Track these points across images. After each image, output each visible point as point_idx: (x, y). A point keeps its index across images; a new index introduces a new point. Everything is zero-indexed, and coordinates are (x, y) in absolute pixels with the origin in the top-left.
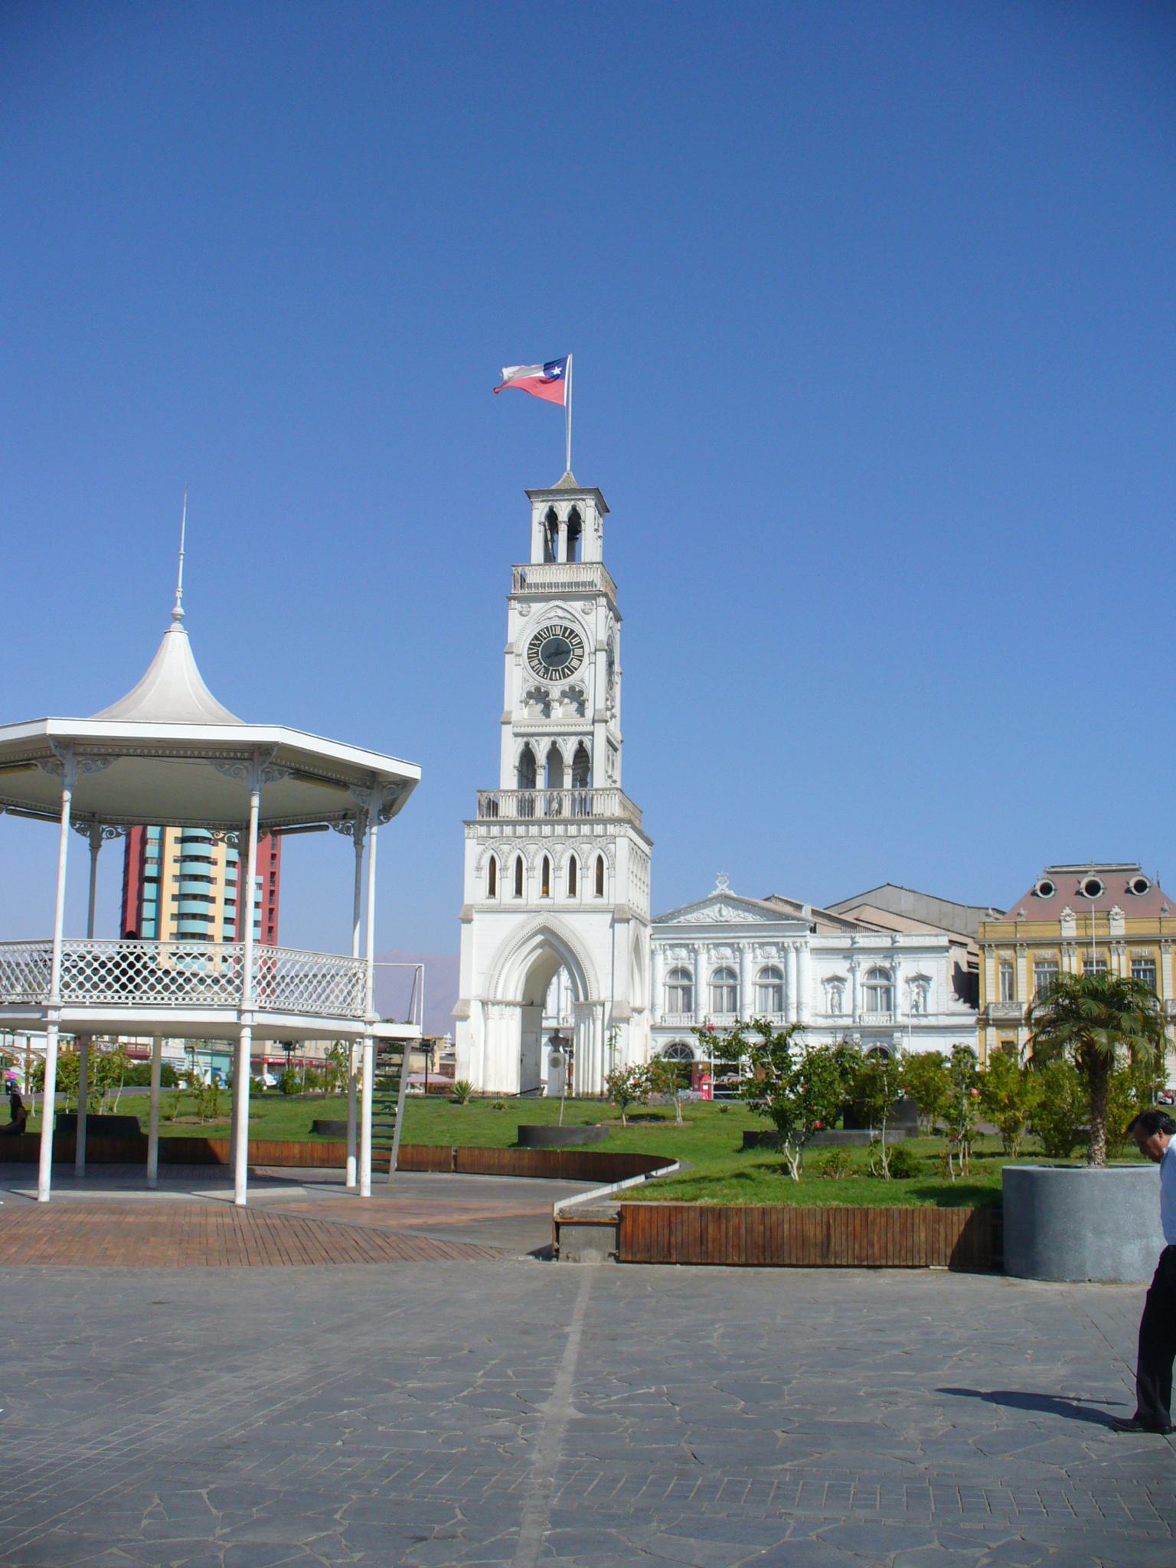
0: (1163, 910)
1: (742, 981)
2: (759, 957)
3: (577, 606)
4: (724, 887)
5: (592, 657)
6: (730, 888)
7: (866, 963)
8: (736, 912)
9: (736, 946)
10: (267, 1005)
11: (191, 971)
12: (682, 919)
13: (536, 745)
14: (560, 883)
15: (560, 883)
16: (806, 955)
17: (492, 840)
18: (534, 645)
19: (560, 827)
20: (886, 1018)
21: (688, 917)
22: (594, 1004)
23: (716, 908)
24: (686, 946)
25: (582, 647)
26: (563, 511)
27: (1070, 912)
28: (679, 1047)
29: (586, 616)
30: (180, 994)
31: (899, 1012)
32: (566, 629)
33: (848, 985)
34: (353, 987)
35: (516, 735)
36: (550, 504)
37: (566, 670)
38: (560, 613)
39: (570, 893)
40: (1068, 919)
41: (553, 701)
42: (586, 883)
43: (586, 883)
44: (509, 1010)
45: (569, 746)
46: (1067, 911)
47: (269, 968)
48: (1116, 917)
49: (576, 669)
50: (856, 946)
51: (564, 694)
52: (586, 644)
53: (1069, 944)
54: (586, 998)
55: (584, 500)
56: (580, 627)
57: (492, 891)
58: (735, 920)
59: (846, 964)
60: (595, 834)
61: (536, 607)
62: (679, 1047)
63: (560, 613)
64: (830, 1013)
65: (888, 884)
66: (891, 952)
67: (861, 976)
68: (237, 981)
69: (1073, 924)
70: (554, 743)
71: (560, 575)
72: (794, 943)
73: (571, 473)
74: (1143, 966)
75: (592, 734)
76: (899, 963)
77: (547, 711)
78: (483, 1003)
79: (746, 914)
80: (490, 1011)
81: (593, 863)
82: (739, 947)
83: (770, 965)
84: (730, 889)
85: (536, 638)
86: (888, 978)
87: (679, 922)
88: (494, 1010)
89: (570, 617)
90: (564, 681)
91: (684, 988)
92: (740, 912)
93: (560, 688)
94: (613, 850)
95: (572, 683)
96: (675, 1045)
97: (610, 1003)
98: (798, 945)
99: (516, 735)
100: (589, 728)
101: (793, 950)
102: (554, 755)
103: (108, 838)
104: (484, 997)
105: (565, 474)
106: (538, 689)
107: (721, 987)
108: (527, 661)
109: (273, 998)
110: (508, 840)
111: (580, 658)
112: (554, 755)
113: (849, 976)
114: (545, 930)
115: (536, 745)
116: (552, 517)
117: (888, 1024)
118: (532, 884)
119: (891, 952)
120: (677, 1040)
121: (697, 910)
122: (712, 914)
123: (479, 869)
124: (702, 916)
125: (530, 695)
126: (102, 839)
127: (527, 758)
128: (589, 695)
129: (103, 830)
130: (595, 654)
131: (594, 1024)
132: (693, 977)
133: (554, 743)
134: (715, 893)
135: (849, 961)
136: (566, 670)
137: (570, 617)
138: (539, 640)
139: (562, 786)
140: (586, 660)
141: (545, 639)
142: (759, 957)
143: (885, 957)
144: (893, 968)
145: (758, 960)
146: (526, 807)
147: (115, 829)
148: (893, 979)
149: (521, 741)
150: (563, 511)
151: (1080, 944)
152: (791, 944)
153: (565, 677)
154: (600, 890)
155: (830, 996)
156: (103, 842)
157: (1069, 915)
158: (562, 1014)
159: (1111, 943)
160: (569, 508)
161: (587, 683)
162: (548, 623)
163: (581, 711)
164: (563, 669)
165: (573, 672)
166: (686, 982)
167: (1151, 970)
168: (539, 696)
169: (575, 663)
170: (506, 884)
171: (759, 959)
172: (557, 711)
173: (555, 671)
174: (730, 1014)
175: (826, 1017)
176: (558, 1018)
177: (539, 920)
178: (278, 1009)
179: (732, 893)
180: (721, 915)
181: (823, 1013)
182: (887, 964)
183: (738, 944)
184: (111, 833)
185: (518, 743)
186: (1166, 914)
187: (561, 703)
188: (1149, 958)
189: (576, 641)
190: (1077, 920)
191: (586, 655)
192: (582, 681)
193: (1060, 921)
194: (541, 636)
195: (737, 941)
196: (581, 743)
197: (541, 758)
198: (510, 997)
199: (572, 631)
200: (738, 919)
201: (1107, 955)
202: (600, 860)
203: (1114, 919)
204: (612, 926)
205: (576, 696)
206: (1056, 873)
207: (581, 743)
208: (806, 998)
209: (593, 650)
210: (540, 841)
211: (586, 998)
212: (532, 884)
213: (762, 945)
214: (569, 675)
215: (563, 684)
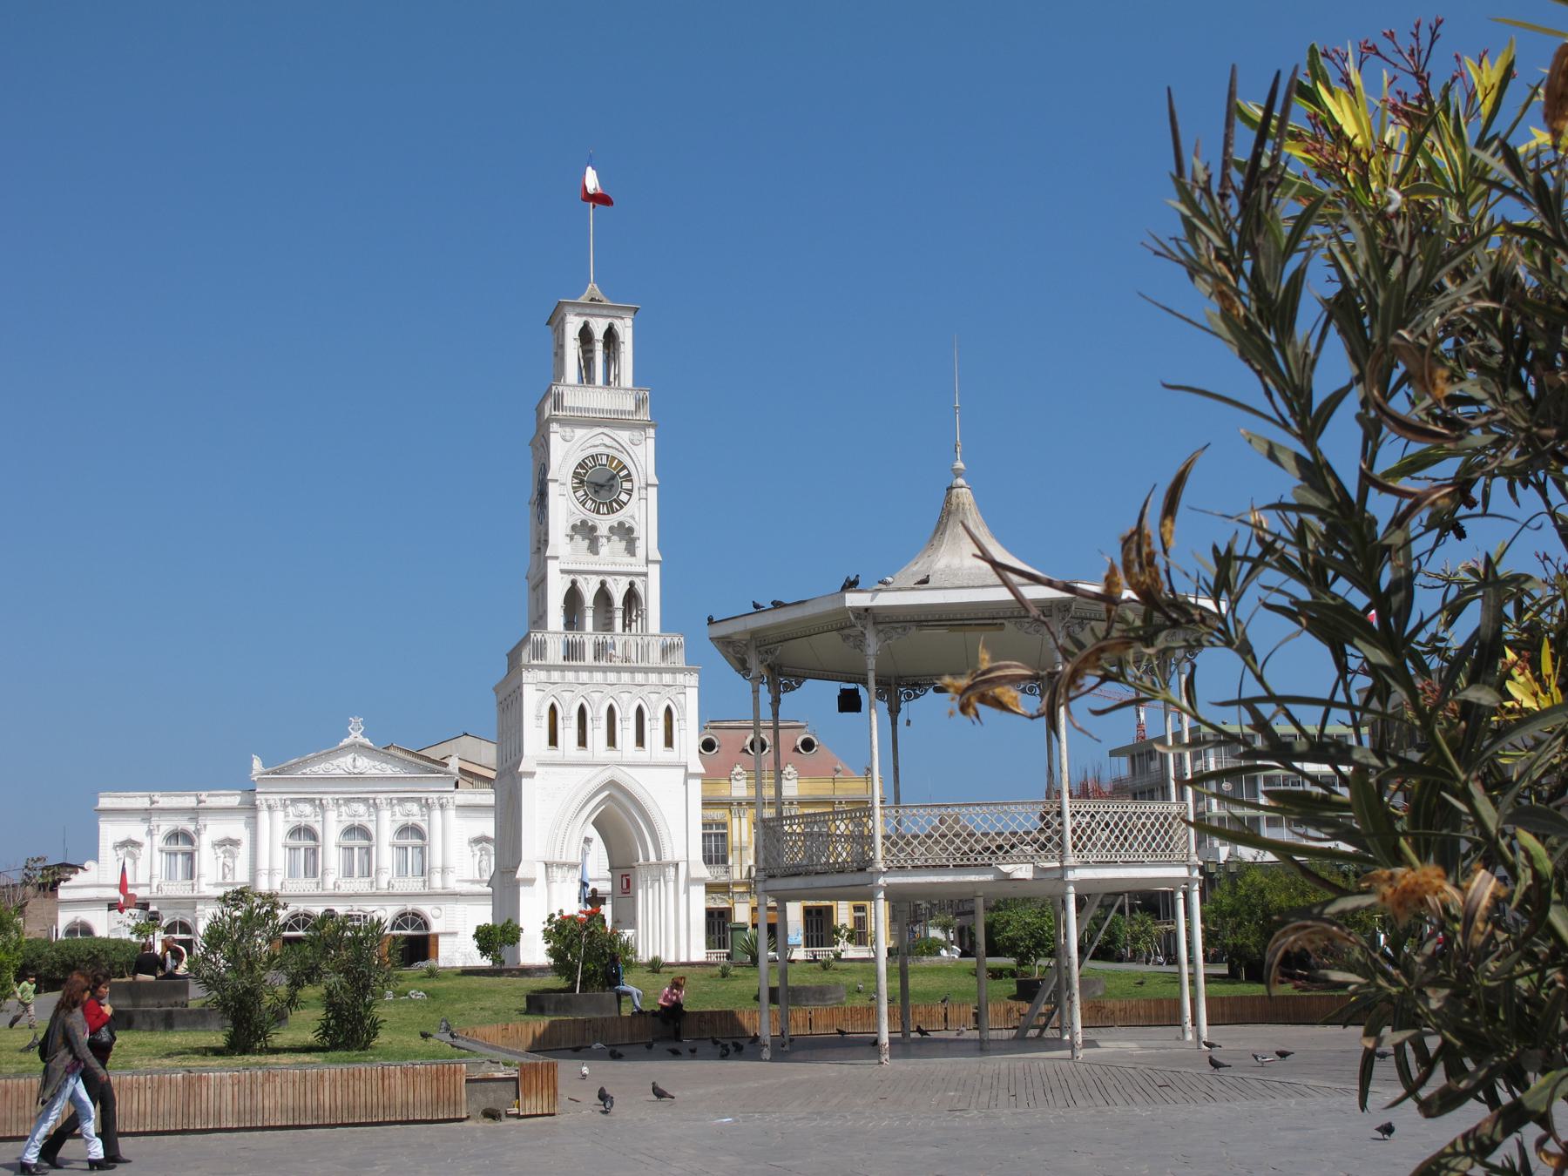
0: (837, 771)
1: (323, 842)
2: (398, 814)
3: (624, 436)
4: (358, 734)
5: (643, 492)
6: (364, 734)
7: (166, 825)
8: (372, 763)
9: (423, 801)
10: (1118, 859)
11: (982, 831)
12: (307, 770)
13: (584, 584)
16: (451, 813)
17: (552, 686)
20: (187, 888)
21: (315, 769)
22: (668, 865)
23: (349, 758)
24: (366, 800)
25: (631, 481)
26: (599, 327)
27: (741, 770)
28: (301, 918)
30: (1000, 854)
31: (203, 881)
32: (614, 458)
33: (145, 850)
35: (563, 571)
36: (584, 319)
38: (608, 441)
39: (551, 744)
40: (738, 777)
45: (620, 586)
46: (738, 769)
47: (1126, 827)
48: (737, 777)
49: (625, 504)
50: (202, 805)
51: (611, 529)
53: (740, 804)
54: (659, 858)
55: (622, 318)
56: (628, 458)
58: (369, 772)
59: (145, 827)
61: (580, 433)
62: (301, 918)
63: (608, 441)
64: (478, 878)
65: (466, 734)
66: (195, 813)
67: (159, 840)
68: (1056, 838)
69: (743, 783)
70: (603, 584)
71: (596, 399)
72: (439, 799)
73: (595, 286)
74: (714, 831)
75: (646, 575)
76: (205, 826)
77: (593, 548)
79: (384, 765)
80: (554, 874)
81: (661, 714)
82: (375, 803)
83: (356, 824)
84: (364, 737)
85: (580, 465)
86: (192, 842)
87: (304, 774)
88: (557, 874)
89: (617, 446)
90: (612, 516)
91: (184, 853)
92: (377, 763)
94: (683, 702)
95: (621, 519)
96: (405, 914)
97: (685, 863)
98: (444, 801)
99: (563, 571)
101: (438, 807)
102: (603, 596)
103: (907, 701)
105: (590, 286)
106: (584, 523)
107: (176, 854)
109: (1113, 852)
111: (630, 492)
112: (603, 596)
113: (146, 841)
114: (612, 784)
115: (584, 584)
116: (585, 335)
117: (190, 894)
119: (195, 813)
120: (301, 910)
121: (326, 761)
122: (343, 766)
123: (539, 717)
124: (331, 768)
125: (574, 527)
126: (901, 701)
127: (573, 599)
128: (639, 532)
129: (901, 693)
131: (666, 885)
132: (320, 839)
133: (603, 584)
134: (346, 741)
137: (617, 446)
138: (584, 468)
139: (546, 628)
140: (635, 494)
141: (591, 468)
142: (398, 814)
143: (191, 819)
144: (198, 832)
145: (342, 818)
146: (573, 651)
147: (914, 691)
148: (196, 844)
149: (568, 579)
150: (599, 327)
151: (750, 804)
152: (436, 801)
154: (669, 742)
155: (477, 859)
156: (782, 696)
157: (739, 774)
158: (155, 883)
159: (732, 804)
161: (637, 519)
162: (594, 451)
163: (631, 550)
165: (621, 508)
166: (188, 848)
167: (723, 835)
168: (585, 531)
169: (624, 497)
171: (398, 816)
172: (604, 548)
173: (603, 504)
174: (363, 880)
175: (473, 882)
176: (150, 885)
177: (605, 775)
178: (1100, 862)
179: (367, 741)
180: (354, 767)
181: (471, 878)
182: (191, 827)
183: (321, 800)
184: (909, 695)
185: (564, 580)
186: (839, 775)
187: (609, 539)
188: (722, 821)
190: (747, 779)
191: (636, 490)
192: (632, 517)
193: (730, 780)
195: (373, 796)
196: (632, 584)
197: (618, 601)
200: (374, 771)
201: (728, 818)
202: (668, 711)
203: (787, 779)
204: (686, 783)
205: (625, 533)
206: (715, 728)
207: (632, 584)
208: (453, 861)
209: (643, 485)
211: (659, 858)
213: (348, 801)
214: (617, 510)
215: (614, 519)
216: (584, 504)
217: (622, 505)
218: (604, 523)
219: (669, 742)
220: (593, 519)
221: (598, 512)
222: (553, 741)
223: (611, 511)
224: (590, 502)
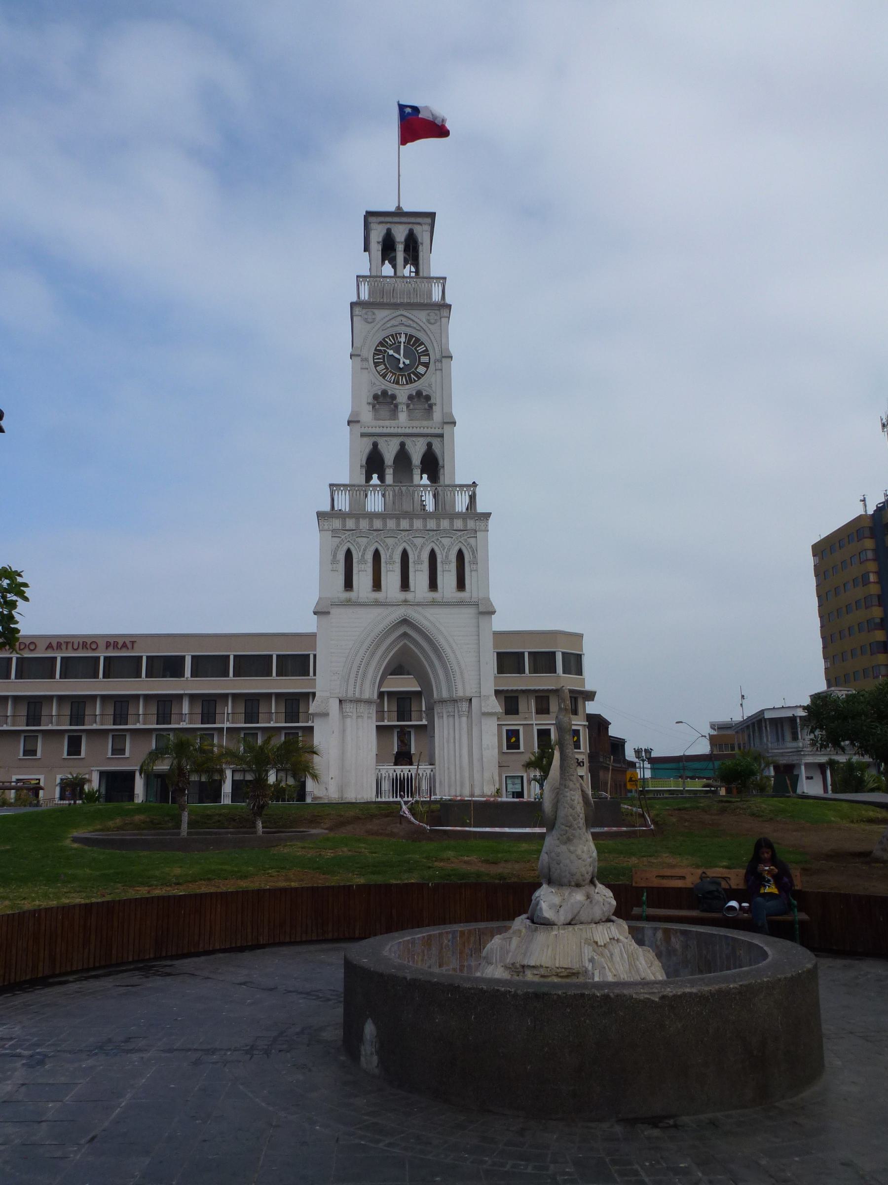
14: (419, 578)
15: (419, 578)
18: (380, 351)
19: (432, 521)
29: (431, 326)
32: (411, 336)
34: (568, 943)
35: (363, 435)
37: (412, 376)
41: (400, 403)
42: (447, 578)
43: (447, 578)
44: (362, 708)
51: (410, 397)
52: (431, 352)
57: (349, 584)
60: (428, 528)
70: (402, 445)
75: (441, 436)
78: (340, 701)
81: (369, 557)
85: (381, 344)
93: (407, 393)
95: (420, 388)
100: (438, 431)
102: (403, 457)
104: (342, 695)
106: (385, 393)
108: (373, 366)
110: (448, 533)
111: (426, 365)
112: (403, 457)
118: (391, 578)
125: (376, 397)
130: (441, 361)
133: (402, 445)
135: (480, 611)
136: (412, 376)
137: (415, 325)
140: (431, 366)
153: (411, 383)
154: (461, 585)
160: (406, 232)
161: (434, 389)
162: (393, 331)
164: (409, 375)
169: (421, 369)
170: (363, 578)
177: (398, 613)
189: (421, 349)
192: (430, 386)
194: (387, 343)
198: (366, 695)
199: (417, 340)
209: (438, 357)
210: (455, 534)
212: (391, 578)
214: (415, 381)
215: (412, 389)
216: (384, 376)
217: (419, 376)
218: (402, 393)
219: (461, 585)
220: (392, 389)
221: (397, 383)
222: (349, 584)
223: (410, 381)
224: (390, 375)
